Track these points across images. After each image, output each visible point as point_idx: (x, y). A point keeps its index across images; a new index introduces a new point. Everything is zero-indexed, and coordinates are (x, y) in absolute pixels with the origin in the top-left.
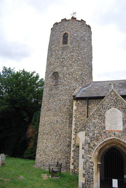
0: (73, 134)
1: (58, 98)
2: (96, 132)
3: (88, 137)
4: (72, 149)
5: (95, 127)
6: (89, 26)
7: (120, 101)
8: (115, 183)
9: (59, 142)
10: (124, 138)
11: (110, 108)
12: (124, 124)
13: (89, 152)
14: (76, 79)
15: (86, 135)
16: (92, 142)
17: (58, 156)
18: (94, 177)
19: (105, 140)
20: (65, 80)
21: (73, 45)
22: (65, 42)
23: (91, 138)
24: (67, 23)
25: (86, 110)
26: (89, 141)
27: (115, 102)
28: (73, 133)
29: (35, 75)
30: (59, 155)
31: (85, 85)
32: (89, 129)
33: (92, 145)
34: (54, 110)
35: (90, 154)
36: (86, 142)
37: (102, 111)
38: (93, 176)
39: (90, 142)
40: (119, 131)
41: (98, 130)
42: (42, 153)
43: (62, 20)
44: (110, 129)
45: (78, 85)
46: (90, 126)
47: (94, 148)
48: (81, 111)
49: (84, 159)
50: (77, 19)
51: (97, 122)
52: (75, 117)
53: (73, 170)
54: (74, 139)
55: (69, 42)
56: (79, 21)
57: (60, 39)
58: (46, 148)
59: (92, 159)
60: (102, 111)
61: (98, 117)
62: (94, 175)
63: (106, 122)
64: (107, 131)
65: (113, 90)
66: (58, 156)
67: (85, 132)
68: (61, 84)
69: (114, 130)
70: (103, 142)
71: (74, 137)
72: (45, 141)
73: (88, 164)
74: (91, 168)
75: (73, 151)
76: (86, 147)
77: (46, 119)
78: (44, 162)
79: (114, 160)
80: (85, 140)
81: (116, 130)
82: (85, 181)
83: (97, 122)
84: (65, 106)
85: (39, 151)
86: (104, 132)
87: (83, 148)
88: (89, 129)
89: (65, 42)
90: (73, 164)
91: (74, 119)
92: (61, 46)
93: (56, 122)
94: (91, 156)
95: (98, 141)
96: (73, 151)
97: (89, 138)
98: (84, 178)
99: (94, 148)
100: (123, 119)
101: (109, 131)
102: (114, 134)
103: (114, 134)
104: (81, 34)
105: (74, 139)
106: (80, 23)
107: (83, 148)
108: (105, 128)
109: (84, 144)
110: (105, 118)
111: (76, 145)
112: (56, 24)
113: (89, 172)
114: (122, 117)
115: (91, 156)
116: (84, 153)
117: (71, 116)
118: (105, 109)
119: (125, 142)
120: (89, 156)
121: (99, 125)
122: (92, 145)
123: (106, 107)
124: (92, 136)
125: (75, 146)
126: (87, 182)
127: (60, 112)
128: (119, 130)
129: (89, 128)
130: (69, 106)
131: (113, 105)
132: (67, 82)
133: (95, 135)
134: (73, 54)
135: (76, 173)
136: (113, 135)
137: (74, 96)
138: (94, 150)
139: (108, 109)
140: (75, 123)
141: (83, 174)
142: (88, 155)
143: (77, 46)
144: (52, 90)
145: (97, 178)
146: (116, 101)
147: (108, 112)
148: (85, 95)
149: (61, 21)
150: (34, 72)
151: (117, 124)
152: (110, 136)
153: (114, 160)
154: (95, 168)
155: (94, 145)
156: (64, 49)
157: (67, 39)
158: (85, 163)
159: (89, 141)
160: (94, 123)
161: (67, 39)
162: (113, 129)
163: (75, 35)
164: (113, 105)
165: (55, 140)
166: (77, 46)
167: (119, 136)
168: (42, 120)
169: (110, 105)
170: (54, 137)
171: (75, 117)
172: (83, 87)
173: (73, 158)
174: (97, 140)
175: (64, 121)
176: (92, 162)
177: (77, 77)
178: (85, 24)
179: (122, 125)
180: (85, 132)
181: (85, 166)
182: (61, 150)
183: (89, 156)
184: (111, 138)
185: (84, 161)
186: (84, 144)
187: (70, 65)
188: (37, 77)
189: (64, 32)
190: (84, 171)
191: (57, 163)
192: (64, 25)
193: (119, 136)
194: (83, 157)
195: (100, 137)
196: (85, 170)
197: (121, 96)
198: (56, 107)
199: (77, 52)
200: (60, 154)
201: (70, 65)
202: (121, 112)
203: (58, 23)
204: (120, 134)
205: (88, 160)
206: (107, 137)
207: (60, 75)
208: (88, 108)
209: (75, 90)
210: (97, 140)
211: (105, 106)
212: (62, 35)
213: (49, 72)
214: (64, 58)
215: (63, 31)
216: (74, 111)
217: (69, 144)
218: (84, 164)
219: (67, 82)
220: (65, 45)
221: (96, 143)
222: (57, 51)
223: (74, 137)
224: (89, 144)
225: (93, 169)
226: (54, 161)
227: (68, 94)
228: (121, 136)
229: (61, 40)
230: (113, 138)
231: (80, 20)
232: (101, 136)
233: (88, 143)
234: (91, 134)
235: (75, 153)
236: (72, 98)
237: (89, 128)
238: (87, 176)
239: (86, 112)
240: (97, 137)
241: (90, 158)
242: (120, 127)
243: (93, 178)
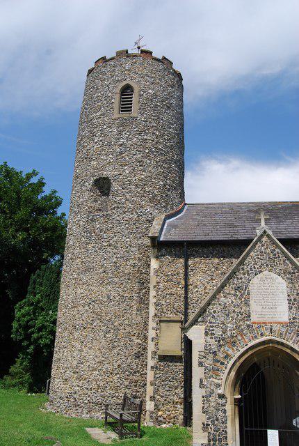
0: (150, 328)
1: (111, 241)
2: (229, 325)
3: (211, 338)
4: (151, 363)
5: (228, 315)
6: (179, 76)
7: (280, 256)
8: (273, 436)
9: (114, 347)
10: (291, 339)
11: (260, 272)
12: (290, 308)
13: (216, 372)
14: (154, 197)
15: (206, 334)
16: (222, 349)
17: (112, 382)
18: (229, 430)
19: (250, 344)
20: (128, 197)
21: (145, 115)
22: (126, 107)
23: (219, 341)
24: (129, 61)
25: (182, 271)
26: (214, 348)
27: (269, 258)
28: (152, 324)
29: (34, 180)
30: (115, 378)
31: (171, 212)
32: (213, 320)
33: (221, 356)
34: (101, 270)
35: (218, 377)
36: (208, 351)
37: (241, 279)
38: (226, 427)
39: (216, 349)
40: (280, 323)
41: (234, 321)
42: (69, 374)
43: (119, 54)
44: (261, 320)
45: (157, 211)
46: (215, 312)
47: (226, 363)
48: (169, 273)
49: (204, 390)
50: (107, 58)
51: (232, 302)
52: (155, 286)
53: (152, 412)
54: (153, 338)
55: (135, 107)
56: (158, 60)
57: (112, 98)
58: (82, 363)
59: (222, 387)
60: (241, 279)
61: (233, 292)
62: (229, 422)
63: (251, 302)
64: (255, 323)
65: (265, 232)
66: (112, 382)
67: (204, 327)
68: (118, 208)
69: (270, 320)
70: (246, 348)
71: (154, 336)
72: (78, 345)
73: (213, 400)
74: (221, 408)
75: (152, 367)
76: (209, 361)
77: (79, 291)
78: (75, 396)
79: (266, 384)
80: (206, 346)
81: (274, 320)
82: (209, 441)
83: (232, 302)
84: (127, 260)
85: (62, 371)
86: (248, 326)
87: (201, 364)
88: (213, 320)
89: (126, 107)
90: (152, 398)
91: (153, 293)
92: (116, 115)
93: (105, 299)
94: (219, 382)
95: (234, 345)
96: (152, 367)
97: (213, 340)
98: (206, 434)
99: (226, 363)
100: (289, 296)
101: (260, 323)
102: (271, 330)
103: (271, 330)
104: (164, 91)
105: (153, 338)
106: (161, 66)
107: (201, 364)
108: (249, 316)
109: (203, 354)
110: (249, 294)
111: (159, 353)
112: (104, 59)
113: (217, 420)
114: (285, 291)
115: (219, 382)
116: (203, 376)
117: (144, 284)
118: (248, 275)
119: (297, 347)
120: (216, 381)
121: (237, 310)
122: (222, 356)
123: (251, 269)
124: (222, 335)
125: (157, 357)
126: (212, 443)
127: (116, 276)
128: (280, 320)
129: (213, 317)
130: (137, 262)
131: (267, 265)
132: (134, 202)
133: (229, 333)
134: (145, 137)
135: (159, 419)
136: (268, 333)
137: (153, 239)
138: (226, 368)
139: (256, 275)
140: (155, 300)
141: (203, 424)
142: (214, 380)
143: (156, 118)
144: (93, 220)
145: (233, 430)
146: (272, 255)
147: (256, 281)
148: (174, 236)
149: (115, 55)
150: (34, 173)
151: (276, 308)
152: (262, 335)
153: (266, 384)
154: (230, 407)
155: (225, 357)
156: (123, 124)
157: (123, 98)
158: (206, 399)
159: (214, 348)
160: (225, 307)
161: (123, 98)
162: (267, 319)
163: (150, 91)
164: (267, 265)
165: (103, 343)
166: (156, 118)
167: (281, 334)
168: (67, 293)
169: (259, 264)
170: (100, 334)
171: (155, 286)
172: (168, 217)
173: (152, 384)
174: (234, 344)
175: (125, 295)
176: (222, 396)
177: (155, 192)
178: (172, 68)
179: (287, 309)
180: (204, 327)
181: (206, 405)
182: (119, 366)
183: (216, 381)
184: (264, 338)
185: (205, 394)
186: (203, 354)
187: (140, 162)
188: (41, 184)
189: (124, 83)
190: (204, 418)
191: (125, 400)
192: (123, 66)
193: (281, 334)
194: (202, 385)
195: (240, 338)
196: (207, 415)
197: (283, 241)
198: (105, 262)
199: (153, 133)
200: (118, 376)
201: (140, 162)
202: (283, 281)
203: (107, 58)
204: (284, 330)
205: (213, 390)
206: (256, 337)
207: (115, 186)
208: (186, 266)
209: (150, 221)
210: (234, 344)
211: (249, 267)
212: (118, 90)
213: (86, 175)
214: (125, 144)
215: (121, 81)
216: (152, 274)
217: (139, 352)
218: (204, 401)
219: (134, 202)
220: (126, 115)
221: (230, 352)
222: (105, 127)
223: (154, 336)
224: (215, 353)
225: (225, 412)
226: (102, 393)
227: (134, 233)
228: (286, 334)
229: (116, 100)
230: (268, 338)
231: (115, 55)
232: (241, 336)
233: (213, 353)
234: (218, 332)
235: (158, 372)
236: (148, 242)
237: (213, 317)
238: (211, 428)
239: (182, 276)
240: (233, 337)
241: (218, 386)
242: (283, 313)
243: (226, 432)
